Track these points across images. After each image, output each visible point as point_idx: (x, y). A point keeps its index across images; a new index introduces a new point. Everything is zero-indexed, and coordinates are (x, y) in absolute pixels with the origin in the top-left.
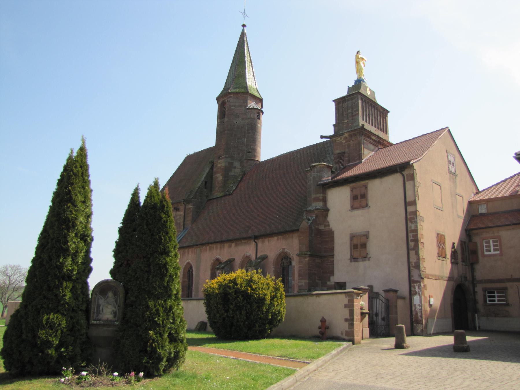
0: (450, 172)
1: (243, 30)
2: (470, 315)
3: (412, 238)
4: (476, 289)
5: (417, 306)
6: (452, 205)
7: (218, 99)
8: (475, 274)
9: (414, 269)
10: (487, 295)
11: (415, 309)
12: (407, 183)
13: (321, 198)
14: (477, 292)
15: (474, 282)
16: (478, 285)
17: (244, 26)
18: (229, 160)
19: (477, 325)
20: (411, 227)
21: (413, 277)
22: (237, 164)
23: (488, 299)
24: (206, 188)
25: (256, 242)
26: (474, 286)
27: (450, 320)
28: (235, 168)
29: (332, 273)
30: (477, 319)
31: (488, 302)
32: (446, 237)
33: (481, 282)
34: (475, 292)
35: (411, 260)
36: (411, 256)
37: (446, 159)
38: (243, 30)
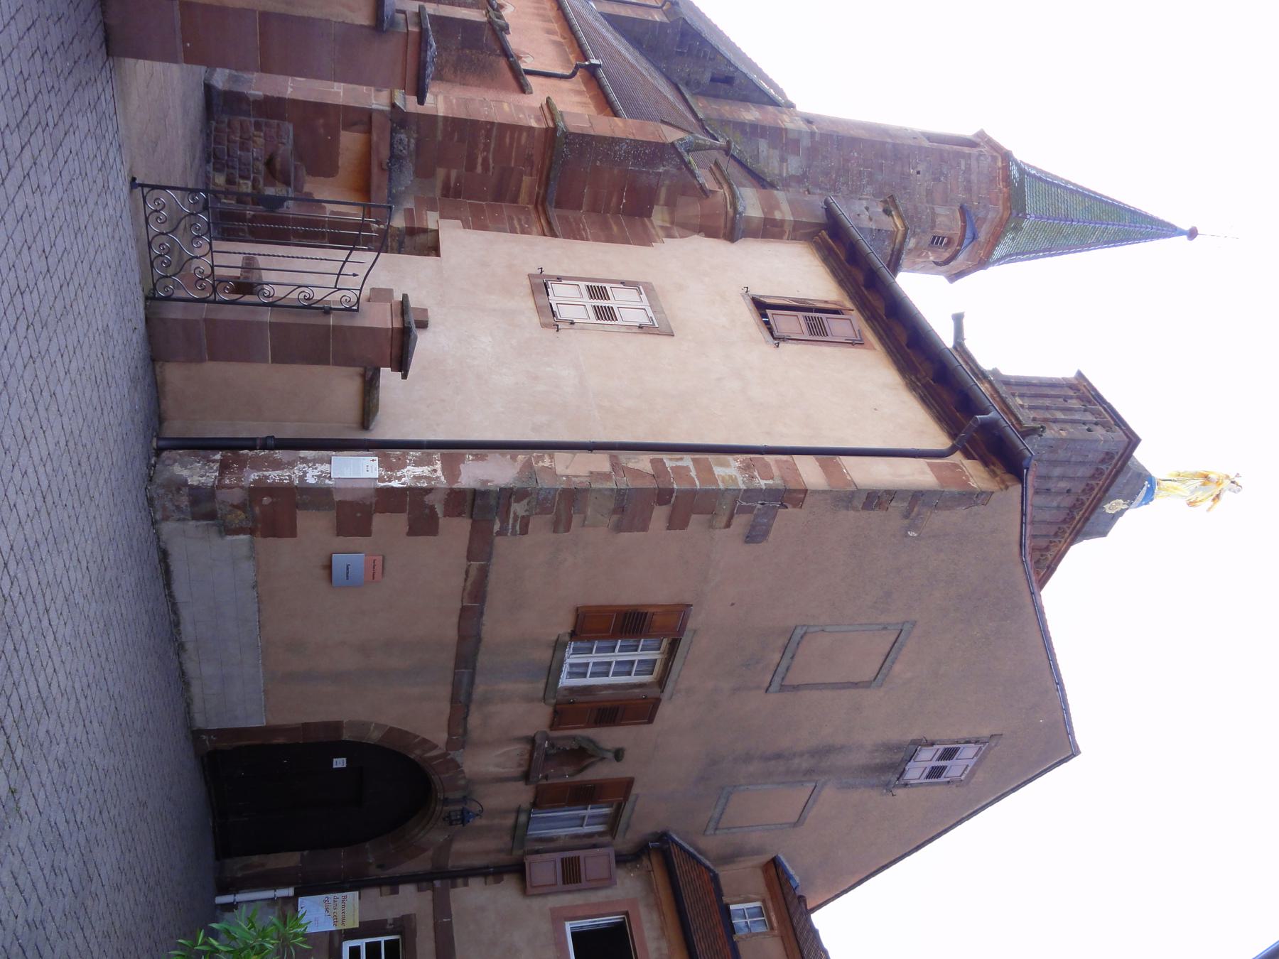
0: (910, 751)
1: (1182, 233)
2: (291, 859)
3: (669, 464)
4: (407, 890)
5: (325, 467)
6: (778, 756)
7: (981, 134)
8: (476, 883)
9: (518, 466)
10: (382, 939)
11: (304, 460)
12: (922, 462)
13: (778, 215)
14: (395, 892)
15: (441, 877)
16: (428, 895)
17: (1192, 234)
18: (805, 142)
19: (241, 897)
20: (726, 465)
21: (478, 458)
22: (794, 165)
23: (362, 943)
24: (713, 80)
25: (573, 74)
26: (417, 879)
27: (258, 721)
28: (783, 160)
29: (477, 222)
30: (269, 894)
31: (347, 946)
32: (645, 729)
33: (442, 909)
34: (393, 884)
35: (561, 456)
36: (582, 456)
37: (965, 734)
38: (1182, 233)
